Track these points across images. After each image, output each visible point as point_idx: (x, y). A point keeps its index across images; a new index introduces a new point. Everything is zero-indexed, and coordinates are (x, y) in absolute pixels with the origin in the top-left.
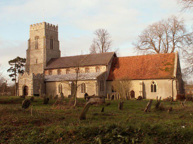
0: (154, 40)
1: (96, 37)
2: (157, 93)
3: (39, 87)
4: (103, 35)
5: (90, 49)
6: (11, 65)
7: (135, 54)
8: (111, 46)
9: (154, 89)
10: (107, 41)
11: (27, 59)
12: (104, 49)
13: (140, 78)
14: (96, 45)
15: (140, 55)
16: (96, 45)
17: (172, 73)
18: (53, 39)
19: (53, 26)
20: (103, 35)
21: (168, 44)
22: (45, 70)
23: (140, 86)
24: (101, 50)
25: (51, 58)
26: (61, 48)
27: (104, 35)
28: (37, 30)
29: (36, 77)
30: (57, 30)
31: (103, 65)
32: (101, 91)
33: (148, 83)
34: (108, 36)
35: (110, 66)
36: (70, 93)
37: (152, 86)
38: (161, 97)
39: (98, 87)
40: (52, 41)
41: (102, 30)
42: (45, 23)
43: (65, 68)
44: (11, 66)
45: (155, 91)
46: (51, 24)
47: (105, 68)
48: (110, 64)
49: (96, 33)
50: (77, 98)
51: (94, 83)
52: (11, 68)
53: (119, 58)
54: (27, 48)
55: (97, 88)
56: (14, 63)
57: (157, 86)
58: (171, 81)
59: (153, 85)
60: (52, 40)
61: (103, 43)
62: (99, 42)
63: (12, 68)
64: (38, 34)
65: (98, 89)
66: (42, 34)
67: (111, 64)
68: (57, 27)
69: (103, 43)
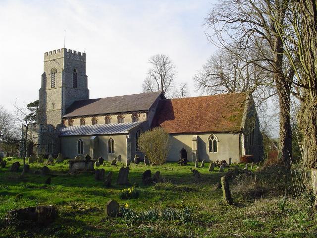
0: (225, 72)
1: (152, 67)
2: (218, 153)
3: (51, 145)
4: (162, 64)
5: (143, 85)
6: (31, 109)
7: (197, 94)
8: (174, 81)
9: (213, 147)
10: (169, 73)
11: (41, 102)
12: (164, 85)
13: (194, 131)
14: (152, 80)
15: (205, 94)
16: (152, 80)
17: (239, 124)
18: (78, 74)
19: (77, 53)
20: (162, 64)
21: (248, 77)
22: (63, 119)
23: (193, 142)
24: (160, 86)
25: (73, 101)
26: (91, 85)
27: (164, 64)
28: (54, 60)
29: (45, 129)
30: (84, 59)
31: (144, 111)
32: (79, 153)
33: (205, 138)
34: (170, 65)
35: (153, 113)
36: (196, 147)
37: (210, 142)
38: (230, 159)
39: (130, 144)
40: (76, 77)
41: (160, 57)
42: (65, 50)
43: (103, 115)
44: (30, 112)
45: (215, 150)
46: (74, 51)
47: (146, 116)
48: (153, 111)
49: (153, 62)
50: (245, 160)
51: (125, 138)
52: (30, 115)
53: (172, 102)
54: (40, 87)
55: (128, 147)
56: (35, 107)
57: (217, 142)
58: (237, 136)
59: (212, 141)
60: (75, 76)
61: (163, 78)
62: (157, 75)
63: (32, 114)
64: (55, 66)
65: (130, 147)
66: (61, 66)
67: (155, 110)
68: (84, 54)
69: (163, 78)
